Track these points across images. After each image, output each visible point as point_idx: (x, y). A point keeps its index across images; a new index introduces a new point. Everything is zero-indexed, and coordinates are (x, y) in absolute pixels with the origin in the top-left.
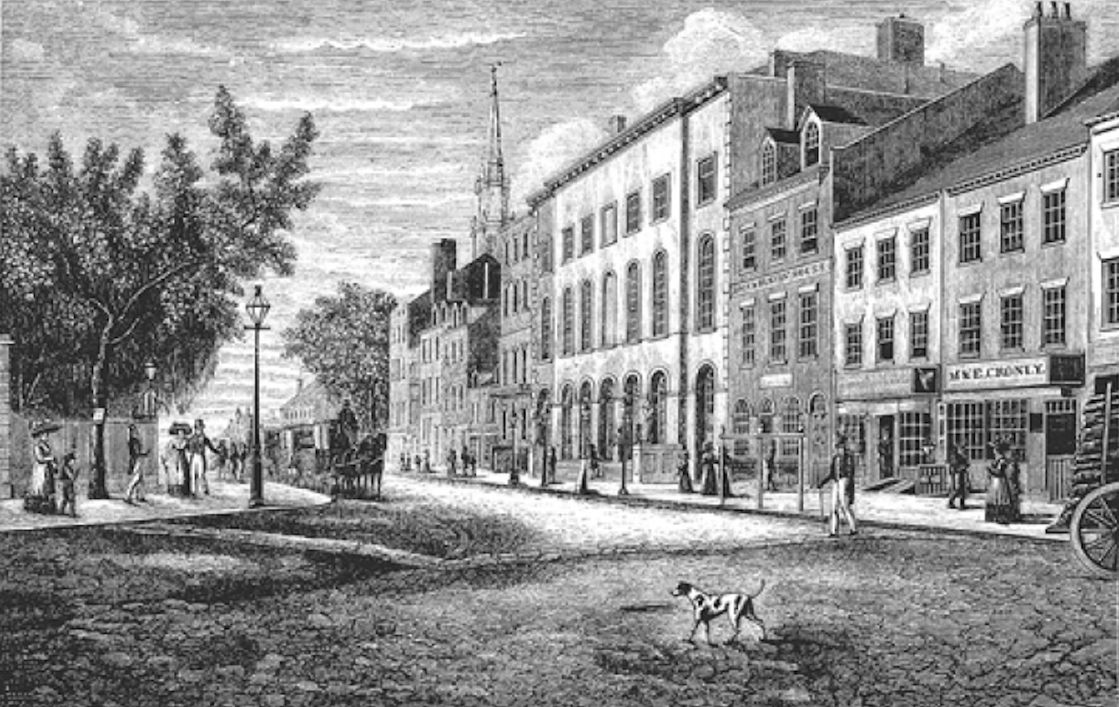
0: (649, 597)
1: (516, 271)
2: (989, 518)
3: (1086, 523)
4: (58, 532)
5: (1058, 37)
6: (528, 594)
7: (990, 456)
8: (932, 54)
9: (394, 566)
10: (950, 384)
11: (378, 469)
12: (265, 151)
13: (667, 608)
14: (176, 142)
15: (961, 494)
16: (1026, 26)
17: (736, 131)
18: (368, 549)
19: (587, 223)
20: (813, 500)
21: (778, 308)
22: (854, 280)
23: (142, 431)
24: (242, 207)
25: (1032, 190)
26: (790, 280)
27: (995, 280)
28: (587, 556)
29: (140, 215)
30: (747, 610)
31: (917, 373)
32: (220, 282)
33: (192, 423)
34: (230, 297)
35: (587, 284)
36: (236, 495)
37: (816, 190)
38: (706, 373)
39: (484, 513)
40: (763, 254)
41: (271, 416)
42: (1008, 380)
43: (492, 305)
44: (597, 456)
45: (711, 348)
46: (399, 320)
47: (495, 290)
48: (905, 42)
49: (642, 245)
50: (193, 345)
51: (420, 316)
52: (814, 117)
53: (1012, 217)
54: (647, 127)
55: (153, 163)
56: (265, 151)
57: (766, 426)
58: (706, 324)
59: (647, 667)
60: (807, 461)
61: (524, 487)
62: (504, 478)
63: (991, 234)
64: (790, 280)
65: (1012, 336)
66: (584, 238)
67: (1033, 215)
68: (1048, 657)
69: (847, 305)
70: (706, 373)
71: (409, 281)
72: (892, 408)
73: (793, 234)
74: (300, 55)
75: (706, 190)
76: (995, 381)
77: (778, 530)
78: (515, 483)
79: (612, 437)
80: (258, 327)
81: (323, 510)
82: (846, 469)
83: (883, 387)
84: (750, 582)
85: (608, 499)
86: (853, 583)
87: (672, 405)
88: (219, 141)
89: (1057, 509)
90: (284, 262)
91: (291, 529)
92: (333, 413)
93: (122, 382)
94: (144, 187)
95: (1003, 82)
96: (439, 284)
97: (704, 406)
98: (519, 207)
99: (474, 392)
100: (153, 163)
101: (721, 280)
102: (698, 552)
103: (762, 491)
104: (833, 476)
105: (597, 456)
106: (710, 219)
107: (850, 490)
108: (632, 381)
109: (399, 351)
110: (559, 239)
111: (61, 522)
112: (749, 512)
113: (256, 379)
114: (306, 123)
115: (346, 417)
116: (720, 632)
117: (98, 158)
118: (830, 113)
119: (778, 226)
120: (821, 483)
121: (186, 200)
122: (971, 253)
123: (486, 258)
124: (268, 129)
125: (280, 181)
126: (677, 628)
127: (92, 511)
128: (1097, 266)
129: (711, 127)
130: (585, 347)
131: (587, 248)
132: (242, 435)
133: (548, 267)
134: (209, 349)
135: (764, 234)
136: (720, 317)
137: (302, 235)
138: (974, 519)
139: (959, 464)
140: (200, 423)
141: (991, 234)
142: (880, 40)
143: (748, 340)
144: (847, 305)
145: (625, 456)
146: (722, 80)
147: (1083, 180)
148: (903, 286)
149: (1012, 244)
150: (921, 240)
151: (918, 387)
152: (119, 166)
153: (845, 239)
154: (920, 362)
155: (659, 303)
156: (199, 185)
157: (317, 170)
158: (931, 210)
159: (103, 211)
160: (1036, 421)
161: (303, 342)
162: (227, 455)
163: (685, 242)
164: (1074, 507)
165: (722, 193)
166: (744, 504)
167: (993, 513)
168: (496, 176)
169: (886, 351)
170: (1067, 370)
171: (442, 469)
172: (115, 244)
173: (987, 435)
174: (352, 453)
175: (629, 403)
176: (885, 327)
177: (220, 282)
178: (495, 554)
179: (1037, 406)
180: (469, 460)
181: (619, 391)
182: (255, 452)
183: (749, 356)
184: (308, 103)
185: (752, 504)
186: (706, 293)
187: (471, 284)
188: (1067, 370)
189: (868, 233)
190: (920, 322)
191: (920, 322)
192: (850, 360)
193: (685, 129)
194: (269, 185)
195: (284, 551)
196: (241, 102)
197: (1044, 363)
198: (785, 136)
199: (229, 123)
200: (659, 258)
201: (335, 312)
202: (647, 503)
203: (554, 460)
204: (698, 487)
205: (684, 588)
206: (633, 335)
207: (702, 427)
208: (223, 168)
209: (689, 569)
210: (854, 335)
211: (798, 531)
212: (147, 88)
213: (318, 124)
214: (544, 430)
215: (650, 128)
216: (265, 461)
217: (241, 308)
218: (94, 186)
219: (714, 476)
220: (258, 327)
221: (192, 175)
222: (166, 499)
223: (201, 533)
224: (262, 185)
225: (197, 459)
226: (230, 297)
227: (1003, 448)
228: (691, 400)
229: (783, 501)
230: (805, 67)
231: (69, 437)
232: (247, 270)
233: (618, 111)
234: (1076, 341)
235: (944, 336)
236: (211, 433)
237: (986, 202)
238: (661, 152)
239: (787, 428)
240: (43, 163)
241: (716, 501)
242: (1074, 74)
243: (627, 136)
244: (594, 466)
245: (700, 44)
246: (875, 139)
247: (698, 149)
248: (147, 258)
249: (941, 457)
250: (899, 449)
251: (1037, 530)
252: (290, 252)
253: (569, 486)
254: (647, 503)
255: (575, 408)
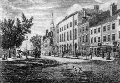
0: (70, 68)
1: (55, 33)
2: (107, 59)
3: (117, 60)
4: (6, 62)
5: (114, 7)
6: (57, 68)
7: (107, 53)
8: (100, 9)
9: (42, 65)
10: (102, 45)
11: (40, 55)
12: (28, 20)
13: (71, 69)
14: (18, 19)
15: (103, 57)
16: (111, 5)
17: (79, 17)
18: (39, 63)
19: (63, 27)
20: (87, 58)
21: (84, 36)
22: (92, 33)
23: (14, 51)
24: (25, 26)
25: (111, 23)
26: (85, 33)
27: (107, 33)
28: (62, 64)
29: (14, 27)
30: (80, 69)
31: (99, 44)
32: (23, 34)
33: (20, 50)
34: (24, 36)
35: (63, 34)
36: (25, 58)
37: (87, 24)
38: (76, 44)
39: (52, 59)
40: (82, 31)
41: (29, 49)
42: (109, 44)
43: (52, 36)
44: (64, 53)
45: (76, 41)
46: (42, 38)
47: (52, 35)
48: (97, 7)
49: (68, 30)
50: (19, 42)
51: (44, 38)
52: (87, 16)
53: (109, 26)
54: (70, 16)
55: (16, 21)
56: (28, 20)
57: (82, 50)
58: (76, 38)
59: (69, 76)
60: (87, 54)
61: (56, 56)
62: (54, 55)
63: (107, 28)
64: (85, 33)
65: (109, 40)
66: (62, 29)
67: (111, 26)
68: (113, 74)
69: (91, 36)
70: (76, 44)
71: (43, 34)
72: (96, 47)
73: (85, 28)
74: (31, 10)
75: (76, 24)
76: (107, 44)
77: (84, 61)
78: (55, 56)
79: (66, 51)
80: (27, 39)
81: (34, 59)
82: (91, 54)
83: (94, 45)
84: (80, 66)
85: (65, 58)
86: (92, 66)
87: (72, 47)
88: (22, 19)
89: (114, 58)
90: (30, 32)
91: (31, 61)
92: (35, 48)
93: (12, 46)
94: (15, 24)
95: (108, 12)
96: (46, 35)
97: (76, 47)
98: (55, 26)
99: (50, 46)
100: (16, 21)
101: (77, 33)
102: (75, 63)
103: (82, 56)
104: (89, 55)
105: (64, 53)
106: (76, 27)
107: (92, 56)
108: (68, 45)
109: (42, 42)
110: (60, 29)
111: (6, 61)
112: (65, 58)
113: (27, 45)
114: (32, 17)
115: (36, 49)
116: (78, 72)
117: (10, 21)
118: (89, 15)
119: (83, 28)
120: (88, 56)
121: (19, 25)
122: (104, 30)
123: (52, 31)
124: (28, 18)
125: (29, 23)
126: (73, 71)
127: (9, 59)
128: (118, 32)
129: (76, 17)
130: (63, 41)
131: (63, 30)
132: (25, 51)
133: (58, 32)
134: (22, 42)
135: (82, 29)
136: (77, 38)
137: (32, 29)
138: (105, 59)
139: (103, 54)
140: (21, 50)
141: (107, 28)
142: (94, 7)
143: (80, 40)
144: (91, 36)
145: (67, 53)
146: (77, 12)
147: (116, 22)
148: (97, 34)
149: (104, 30)
150: (99, 29)
151: (99, 45)
152: (11, 22)
153: (91, 29)
154: (99, 42)
155: (71, 36)
156: (20, 24)
157: (33, 22)
158: (100, 26)
159: (10, 27)
160: (112, 49)
161: (32, 41)
162: (24, 53)
163: (73, 30)
164: (116, 58)
165: (77, 24)
166: (80, 58)
167: (107, 59)
168: (53, 22)
169: (95, 41)
170: (115, 43)
171: (47, 55)
172: (11, 30)
173: (106, 50)
174: (37, 53)
175: (67, 47)
176: (95, 38)
177: (23, 34)
178: (53, 64)
179: (112, 47)
180: (50, 54)
181: (66, 46)
182: (27, 53)
183: (80, 42)
184: (32, 15)
185: (81, 58)
186: (76, 35)
187: (49, 34)
188: (115, 43)
189: (93, 29)
190: (99, 38)
191: (99, 38)
192: (91, 42)
193: (73, 17)
194: (29, 24)
195: (30, 63)
196: (25, 15)
197: (112, 42)
198: (84, 18)
199: (24, 17)
200: (71, 31)
201: (35, 37)
202: (69, 58)
203: (59, 53)
204: (75, 56)
205: (74, 67)
206: (68, 40)
207: (75, 50)
208: (23, 22)
209: (74, 65)
210: (92, 39)
211: (86, 61)
212: (15, 13)
213: (33, 17)
214: (58, 50)
215: (68, 17)
216: (28, 54)
217: (25, 37)
218: (9, 24)
219: (77, 55)
220: (27, 39)
221: (20, 23)
222: (17, 58)
223: (21, 62)
224: (27, 24)
225: (20, 54)
226: (24, 36)
227: (108, 52)
228: (74, 47)
229: (84, 58)
230: (86, 11)
231: (7, 51)
232: (25, 33)
233: (66, 15)
234: (116, 40)
235: (102, 39)
236: (22, 51)
237: (106, 25)
238: (70, 20)
239: (85, 50)
240: (4, 22)
241: (77, 58)
242: (115, 11)
243: (67, 18)
244: (64, 54)
245: (76, 7)
246: (98, 18)
247: (75, 19)
248: (15, 32)
249: (102, 53)
250: (97, 52)
251: (112, 61)
252: (30, 31)
253: (61, 56)
254: (69, 58)
255: (62, 48)
